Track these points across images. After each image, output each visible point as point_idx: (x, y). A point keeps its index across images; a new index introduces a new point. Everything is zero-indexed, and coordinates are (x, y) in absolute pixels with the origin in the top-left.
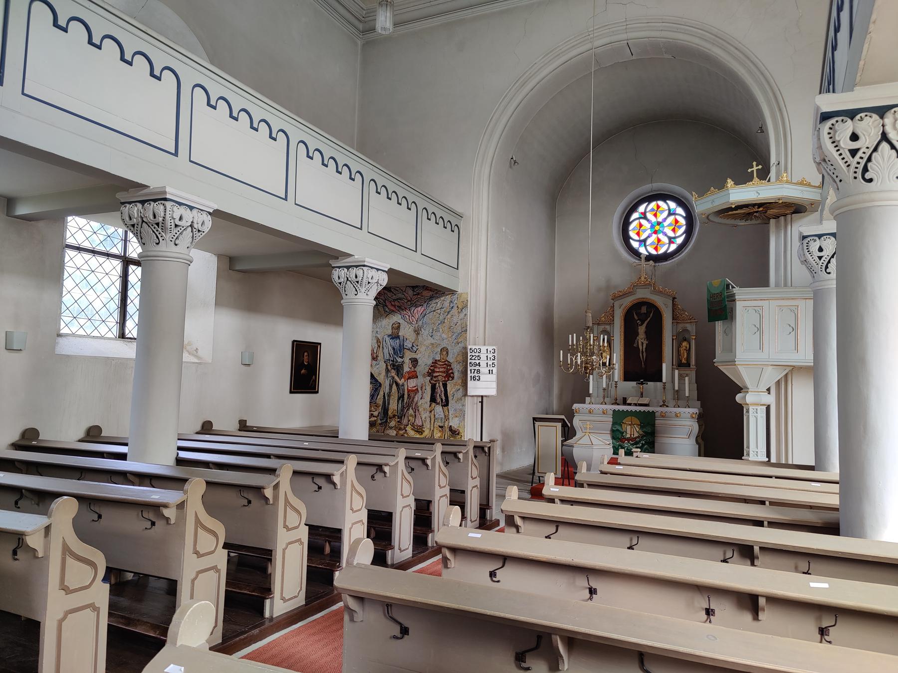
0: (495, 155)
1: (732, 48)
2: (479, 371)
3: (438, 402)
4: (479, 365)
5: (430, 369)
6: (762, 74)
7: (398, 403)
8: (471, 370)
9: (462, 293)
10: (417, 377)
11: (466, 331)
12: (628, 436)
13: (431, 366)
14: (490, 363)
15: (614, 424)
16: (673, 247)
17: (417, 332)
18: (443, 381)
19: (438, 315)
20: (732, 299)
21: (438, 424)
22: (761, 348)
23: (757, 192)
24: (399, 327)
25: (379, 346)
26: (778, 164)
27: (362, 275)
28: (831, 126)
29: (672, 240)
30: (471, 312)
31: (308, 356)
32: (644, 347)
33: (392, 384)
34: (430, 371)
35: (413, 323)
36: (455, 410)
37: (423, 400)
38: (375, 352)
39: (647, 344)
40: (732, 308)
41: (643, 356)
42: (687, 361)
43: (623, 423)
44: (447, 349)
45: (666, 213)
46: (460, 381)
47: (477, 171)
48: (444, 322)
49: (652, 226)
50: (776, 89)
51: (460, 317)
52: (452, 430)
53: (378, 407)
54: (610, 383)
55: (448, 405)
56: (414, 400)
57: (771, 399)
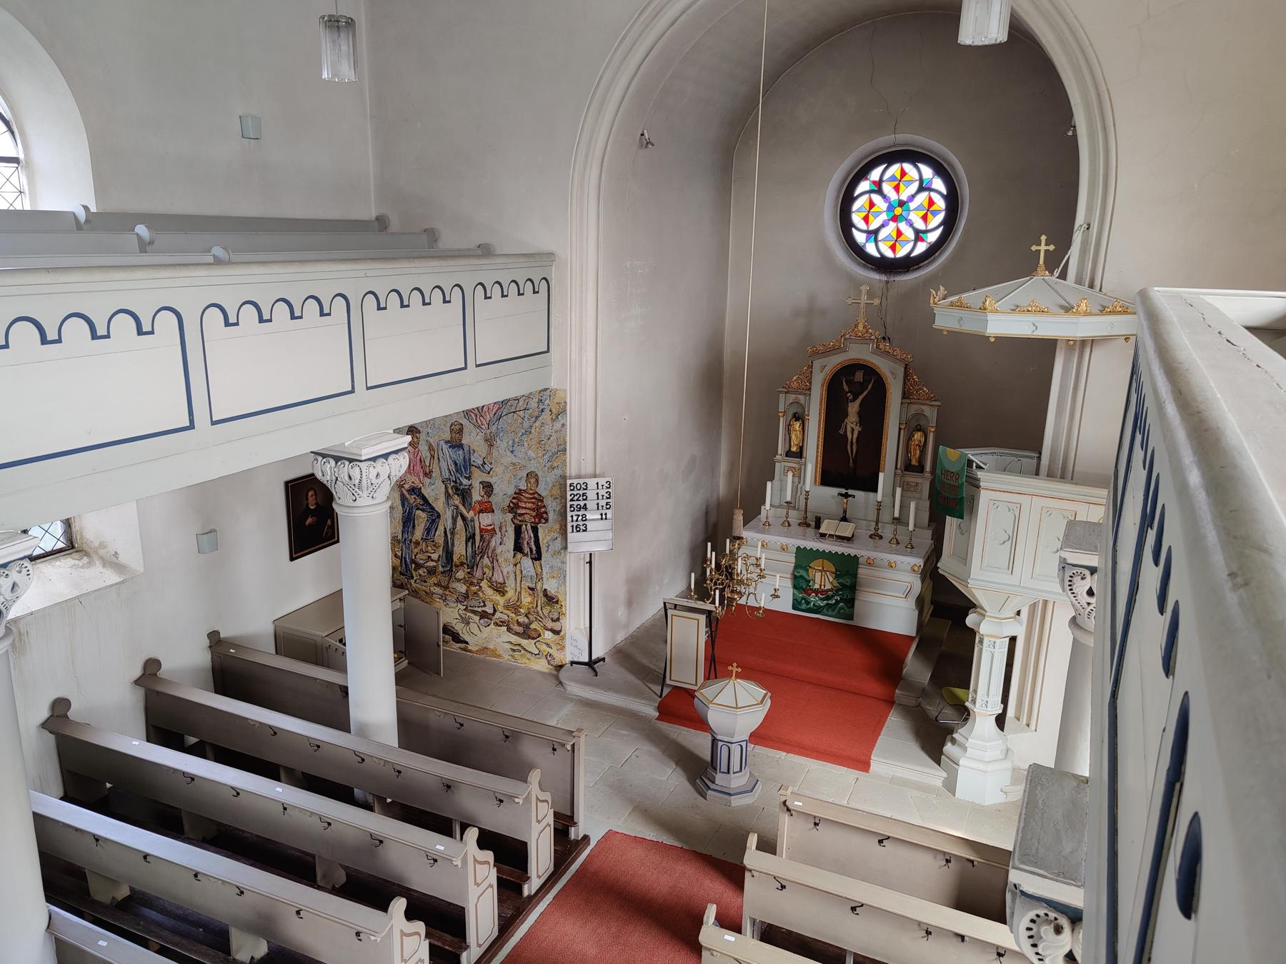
0: (609, 147)
2: (584, 518)
4: (585, 507)
5: (511, 501)
6: (1083, 51)
7: (467, 546)
8: (572, 516)
9: (557, 390)
10: (493, 512)
11: (565, 450)
12: (817, 586)
14: (603, 503)
15: (797, 567)
16: (921, 248)
17: (490, 441)
18: (532, 522)
19: (520, 420)
20: (975, 484)
21: (527, 584)
22: (1011, 567)
23: (1034, 324)
24: (461, 431)
25: (433, 457)
26: (1088, 229)
27: (359, 476)
28: (1035, 918)
30: (573, 422)
31: (316, 494)
32: (855, 436)
33: (457, 517)
34: (511, 505)
35: (483, 427)
36: (552, 567)
37: (504, 546)
38: (428, 465)
39: (859, 432)
40: (973, 496)
41: (852, 449)
43: (810, 567)
44: (537, 475)
45: (915, 186)
47: (576, 176)
49: (891, 208)
50: (1103, 88)
51: (555, 428)
53: (438, 547)
54: (799, 486)
57: (1019, 630)
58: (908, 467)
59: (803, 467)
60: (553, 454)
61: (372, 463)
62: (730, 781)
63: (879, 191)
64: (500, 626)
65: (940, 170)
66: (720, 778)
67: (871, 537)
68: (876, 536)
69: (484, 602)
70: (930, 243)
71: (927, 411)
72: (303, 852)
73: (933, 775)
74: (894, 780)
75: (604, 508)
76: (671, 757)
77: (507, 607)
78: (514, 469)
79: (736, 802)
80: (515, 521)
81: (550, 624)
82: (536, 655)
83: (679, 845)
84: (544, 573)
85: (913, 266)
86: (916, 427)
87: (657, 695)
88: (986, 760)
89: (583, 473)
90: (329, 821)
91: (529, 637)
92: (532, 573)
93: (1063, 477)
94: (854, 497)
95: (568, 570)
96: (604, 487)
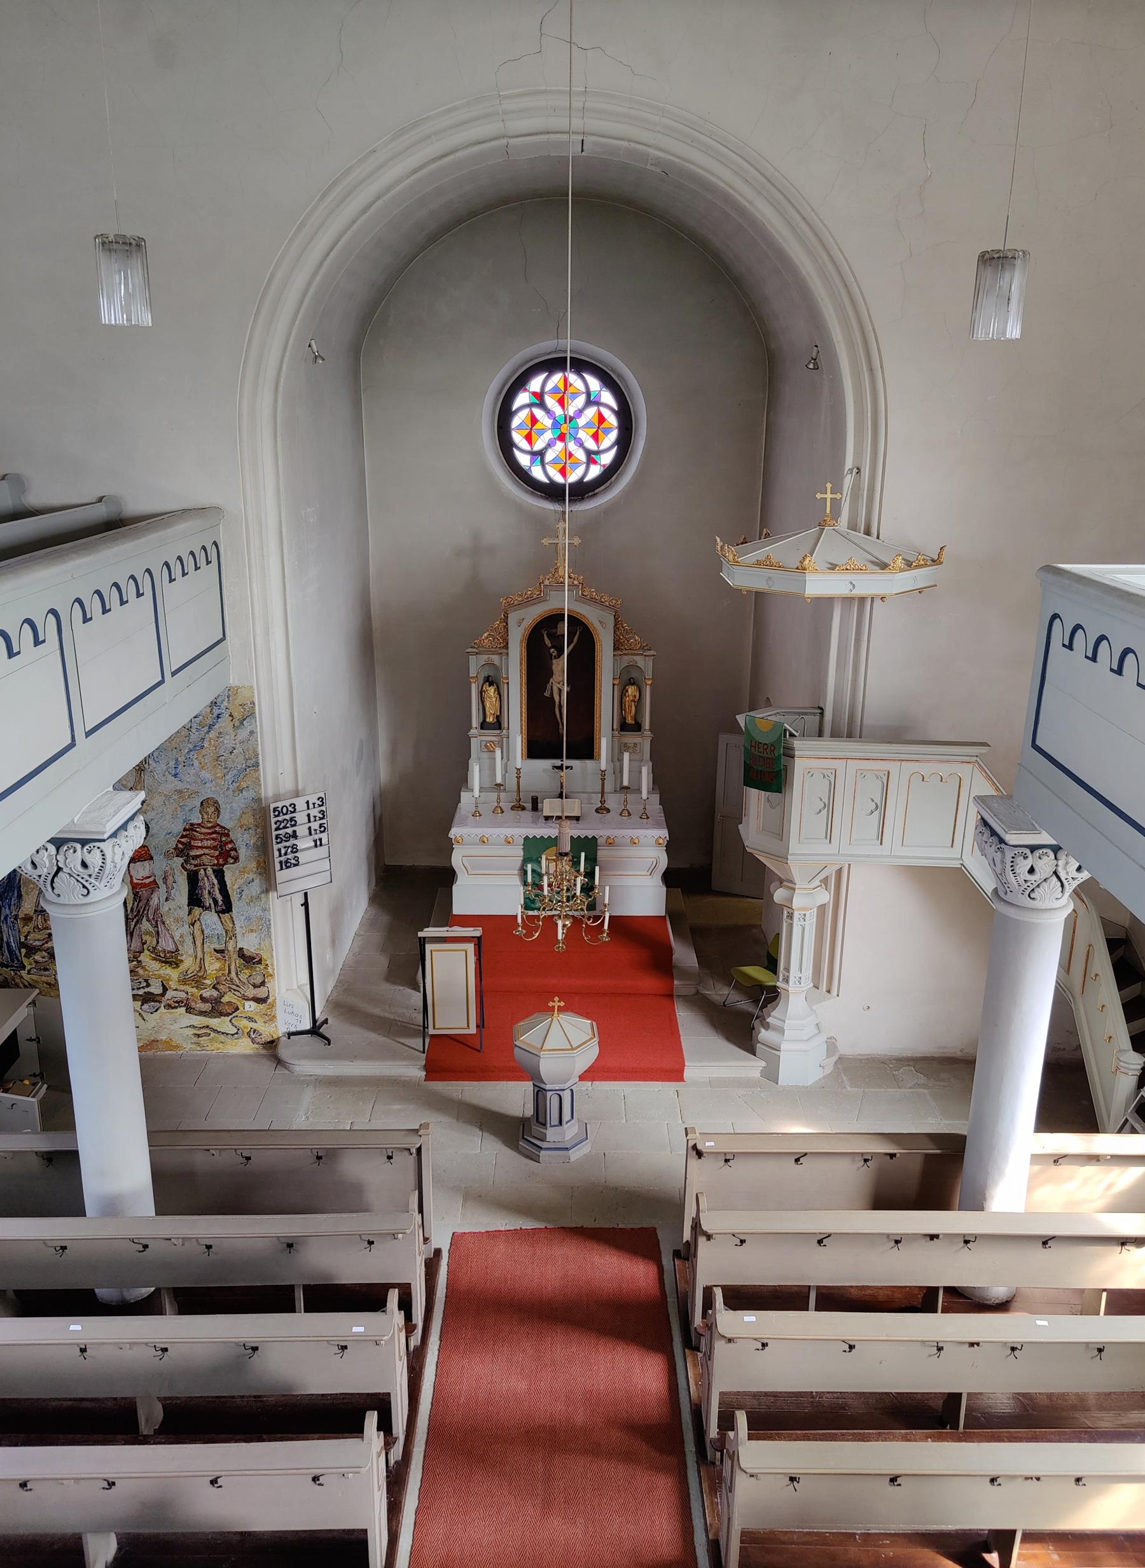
1: (797, 216)
2: (295, 849)
3: (208, 905)
4: (294, 835)
5: (179, 841)
8: (279, 850)
10: (152, 858)
11: (257, 765)
13: (183, 837)
14: (315, 825)
16: (595, 472)
18: (214, 865)
20: (790, 754)
21: (212, 946)
23: (851, 583)
29: (593, 456)
34: (180, 846)
36: (248, 919)
42: (635, 720)
44: (216, 802)
46: (254, 864)
48: (202, 747)
49: (556, 425)
51: (239, 738)
52: (244, 955)
55: (231, 911)
56: (151, 903)
58: (624, 727)
59: (505, 739)
60: (240, 772)
61: (114, 840)
62: (565, 1133)
63: (542, 405)
64: (176, 1007)
65: (609, 381)
66: (552, 1134)
67: (597, 811)
68: (602, 810)
69: (146, 981)
70: (604, 466)
71: (640, 661)
72: (75, 1400)
73: (750, 1067)
74: (712, 1083)
75: (318, 832)
76: (469, 1122)
77: (183, 981)
78: (180, 798)
79: (575, 1155)
80: (188, 867)
81: (251, 992)
82: (233, 1035)
83: (541, 1225)
84: (237, 928)
85: (588, 493)
86: (630, 680)
87: (420, 1051)
88: (806, 1038)
89: (282, 791)
90: (164, 1346)
91: (222, 1014)
92: (220, 930)
93: (850, 735)
94: (572, 769)
95: (272, 918)
96: (316, 805)
